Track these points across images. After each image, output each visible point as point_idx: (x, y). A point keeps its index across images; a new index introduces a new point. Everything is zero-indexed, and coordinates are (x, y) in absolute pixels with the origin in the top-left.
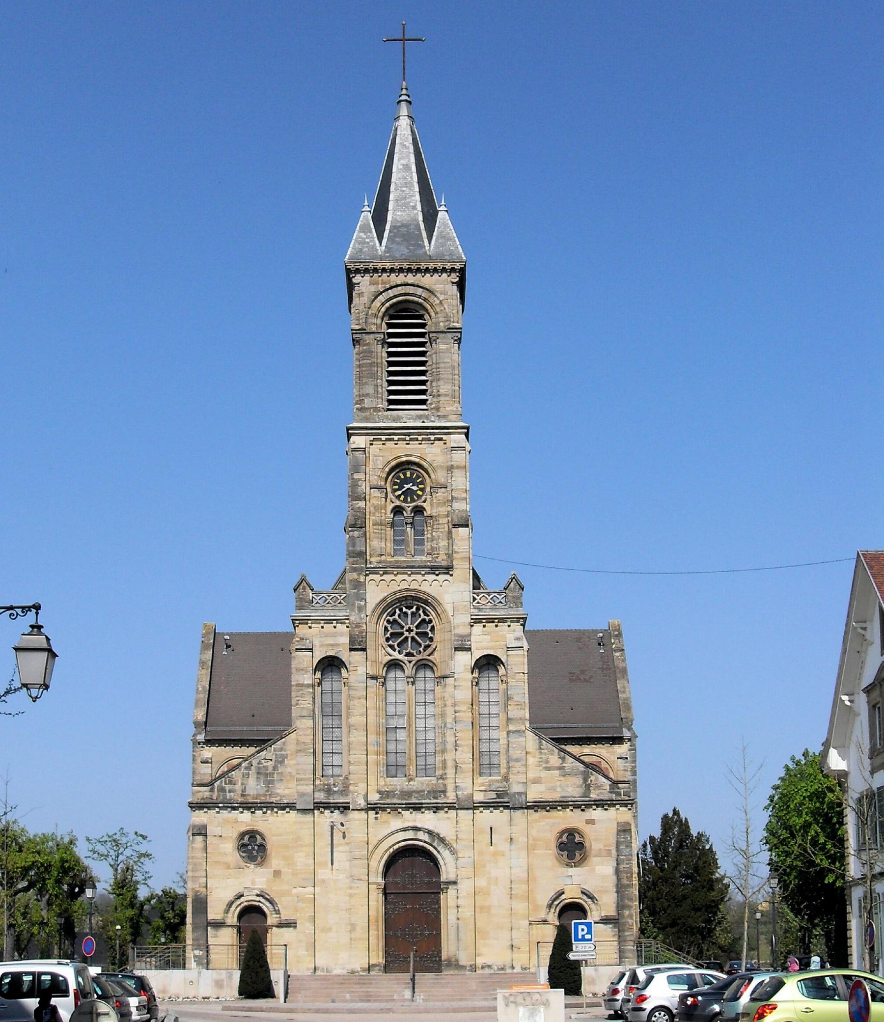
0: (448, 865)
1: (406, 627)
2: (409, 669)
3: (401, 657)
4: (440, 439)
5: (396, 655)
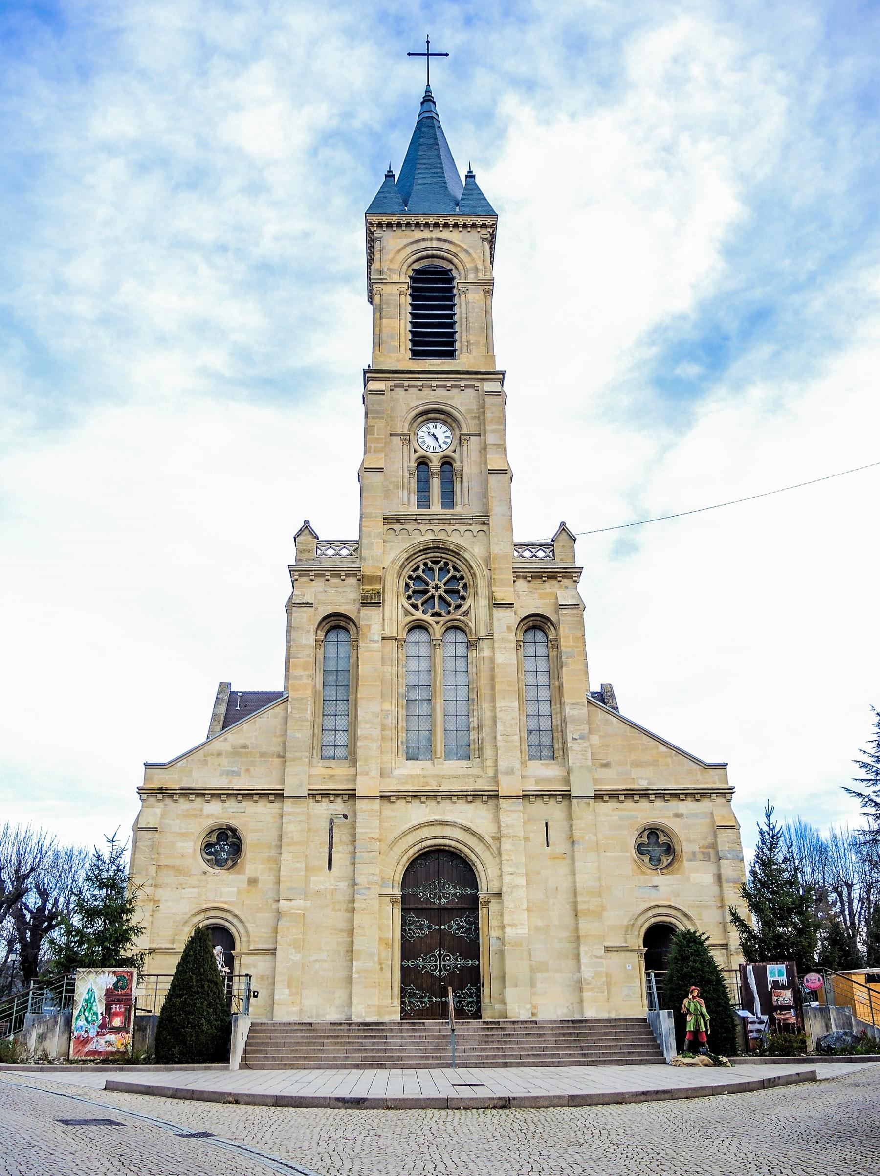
0: (489, 871)
1: (432, 584)
2: (437, 630)
3: (428, 618)
4: (473, 386)
5: (419, 615)
